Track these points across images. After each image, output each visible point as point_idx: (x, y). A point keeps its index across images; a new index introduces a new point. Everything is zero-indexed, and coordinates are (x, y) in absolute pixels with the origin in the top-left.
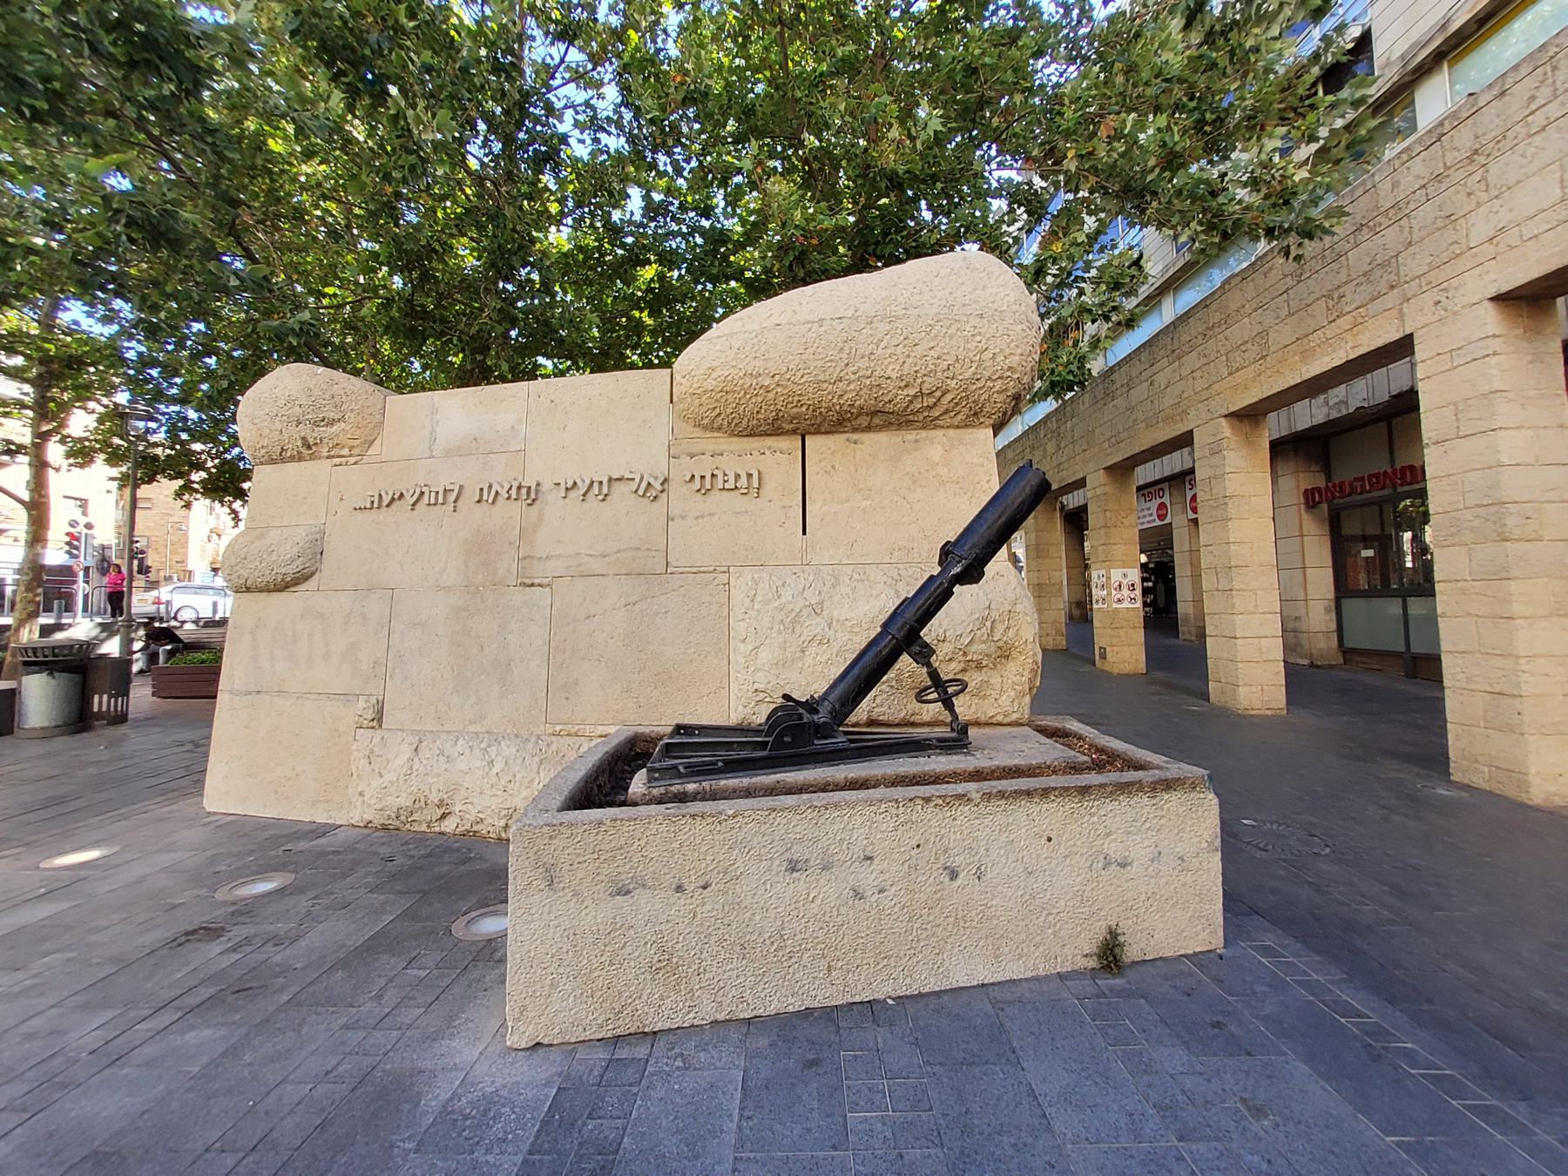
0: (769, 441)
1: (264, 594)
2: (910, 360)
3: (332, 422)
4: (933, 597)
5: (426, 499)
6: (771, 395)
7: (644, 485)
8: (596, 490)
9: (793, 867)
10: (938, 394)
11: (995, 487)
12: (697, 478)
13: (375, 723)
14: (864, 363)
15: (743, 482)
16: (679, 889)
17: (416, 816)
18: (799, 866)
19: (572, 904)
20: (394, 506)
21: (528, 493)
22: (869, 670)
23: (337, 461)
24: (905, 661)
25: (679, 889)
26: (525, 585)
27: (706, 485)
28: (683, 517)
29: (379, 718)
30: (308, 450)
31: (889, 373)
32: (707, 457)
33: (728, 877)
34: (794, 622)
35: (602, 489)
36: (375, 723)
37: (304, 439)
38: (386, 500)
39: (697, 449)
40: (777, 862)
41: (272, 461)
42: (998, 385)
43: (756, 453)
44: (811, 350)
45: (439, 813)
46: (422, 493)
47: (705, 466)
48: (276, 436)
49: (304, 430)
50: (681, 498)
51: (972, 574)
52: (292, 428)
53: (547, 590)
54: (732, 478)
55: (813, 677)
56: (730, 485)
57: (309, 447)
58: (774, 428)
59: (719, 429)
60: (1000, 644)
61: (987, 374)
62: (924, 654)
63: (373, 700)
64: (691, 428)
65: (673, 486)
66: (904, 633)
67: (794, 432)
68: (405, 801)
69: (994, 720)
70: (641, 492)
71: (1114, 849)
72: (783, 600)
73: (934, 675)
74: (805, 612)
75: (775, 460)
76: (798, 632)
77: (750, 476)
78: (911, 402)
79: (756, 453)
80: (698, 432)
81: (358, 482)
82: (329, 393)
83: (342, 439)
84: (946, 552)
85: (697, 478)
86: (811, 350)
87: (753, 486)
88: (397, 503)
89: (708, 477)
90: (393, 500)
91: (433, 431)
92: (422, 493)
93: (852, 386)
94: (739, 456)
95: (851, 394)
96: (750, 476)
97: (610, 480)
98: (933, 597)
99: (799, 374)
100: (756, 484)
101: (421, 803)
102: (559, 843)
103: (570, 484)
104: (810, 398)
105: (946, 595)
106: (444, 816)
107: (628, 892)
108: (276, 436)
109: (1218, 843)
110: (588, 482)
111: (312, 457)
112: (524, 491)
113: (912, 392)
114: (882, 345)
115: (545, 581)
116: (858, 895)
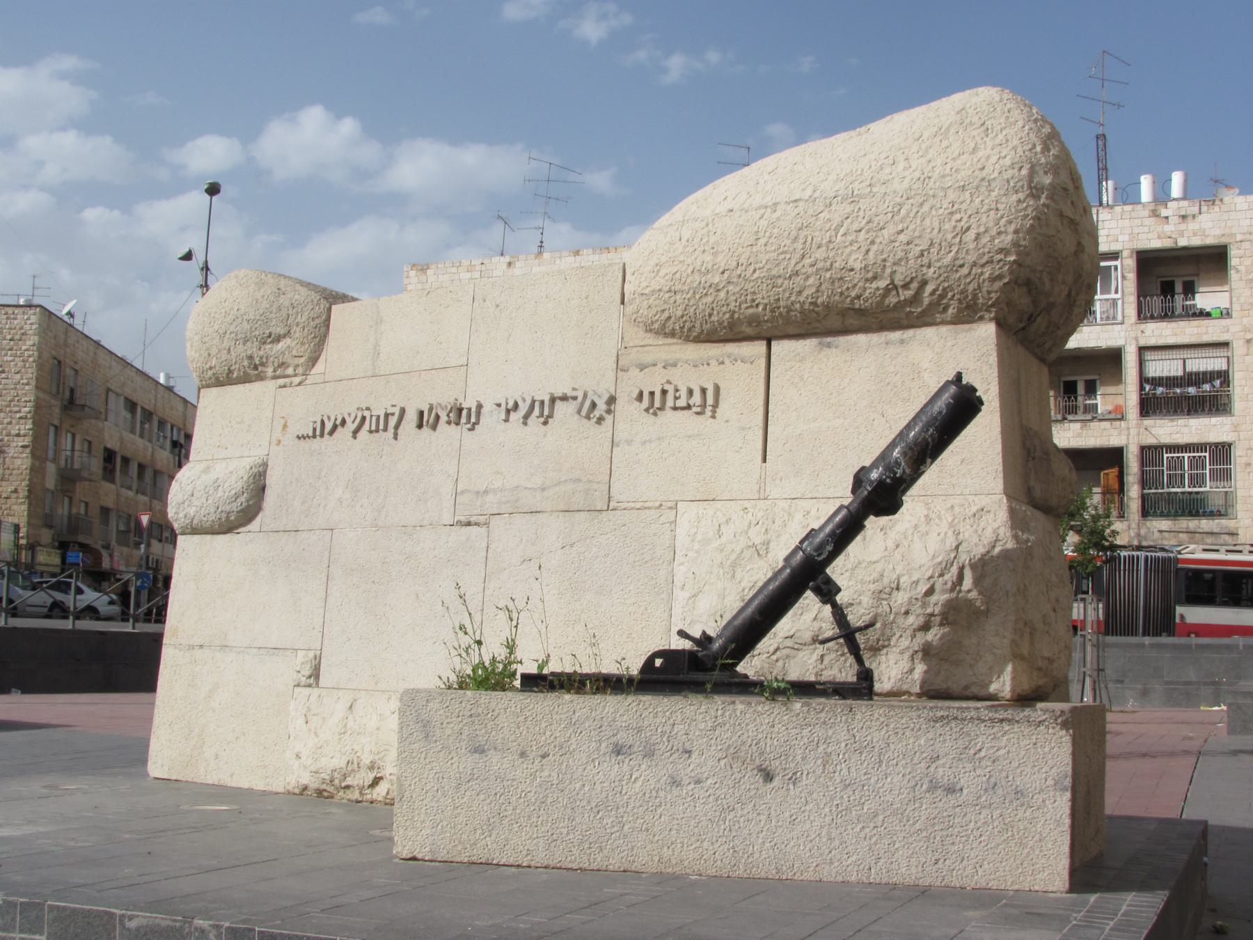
0: (731, 348)
1: (209, 537)
2: (874, 248)
3: (278, 339)
4: (847, 530)
5: (366, 426)
6: (722, 294)
7: (587, 404)
8: (537, 411)
9: (618, 750)
10: (914, 285)
13: (312, 681)
14: (820, 254)
15: (697, 399)
17: (349, 781)
18: (624, 750)
19: (442, 754)
20: (335, 435)
23: (281, 381)
26: (460, 523)
27: (655, 402)
28: (629, 442)
29: (316, 674)
30: (251, 373)
31: (851, 262)
33: (563, 751)
34: (734, 566)
36: (312, 681)
37: (251, 358)
40: (604, 745)
41: (218, 383)
42: (987, 272)
43: (713, 363)
44: (762, 241)
46: (364, 418)
47: (653, 381)
48: (224, 356)
49: (252, 348)
50: (628, 409)
52: (241, 348)
53: (483, 530)
55: (708, 611)
56: (682, 403)
57: (256, 368)
59: (672, 334)
61: (971, 258)
62: (828, 592)
63: (311, 654)
64: (641, 334)
65: (619, 406)
66: (808, 574)
68: (339, 762)
69: (968, 693)
70: (584, 412)
71: (942, 773)
72: (724, 539)
73: (839, 615)
74: (747, 554)
76: (738, 576)
77: (704, 391)
79: (713, 363)
80: (650, 339)
81: (302, 403)
82: (275, 306)
83: (287, 358)
86: (762, 241)
87: (707, 402)
88: (339, 429)
91: (376, 346)
92: (364, 418)
93: (811, 281)
94: (693, 365)
95: (808, 290)
96: (704, 391)
99: (751, 268)
100: (710, 400)
101: (352, 766)
103: (511, 405)
104: (764, 296)
106: (376, 782)
107: (483, 751)
108: (224, 356)
109: (1068, 782)
110: (529, 402)
111: (260, 378)
112: (464, 413)
113: (882, 284)
114: (842, 231)
115: (482, 519)
116: (675, 783)
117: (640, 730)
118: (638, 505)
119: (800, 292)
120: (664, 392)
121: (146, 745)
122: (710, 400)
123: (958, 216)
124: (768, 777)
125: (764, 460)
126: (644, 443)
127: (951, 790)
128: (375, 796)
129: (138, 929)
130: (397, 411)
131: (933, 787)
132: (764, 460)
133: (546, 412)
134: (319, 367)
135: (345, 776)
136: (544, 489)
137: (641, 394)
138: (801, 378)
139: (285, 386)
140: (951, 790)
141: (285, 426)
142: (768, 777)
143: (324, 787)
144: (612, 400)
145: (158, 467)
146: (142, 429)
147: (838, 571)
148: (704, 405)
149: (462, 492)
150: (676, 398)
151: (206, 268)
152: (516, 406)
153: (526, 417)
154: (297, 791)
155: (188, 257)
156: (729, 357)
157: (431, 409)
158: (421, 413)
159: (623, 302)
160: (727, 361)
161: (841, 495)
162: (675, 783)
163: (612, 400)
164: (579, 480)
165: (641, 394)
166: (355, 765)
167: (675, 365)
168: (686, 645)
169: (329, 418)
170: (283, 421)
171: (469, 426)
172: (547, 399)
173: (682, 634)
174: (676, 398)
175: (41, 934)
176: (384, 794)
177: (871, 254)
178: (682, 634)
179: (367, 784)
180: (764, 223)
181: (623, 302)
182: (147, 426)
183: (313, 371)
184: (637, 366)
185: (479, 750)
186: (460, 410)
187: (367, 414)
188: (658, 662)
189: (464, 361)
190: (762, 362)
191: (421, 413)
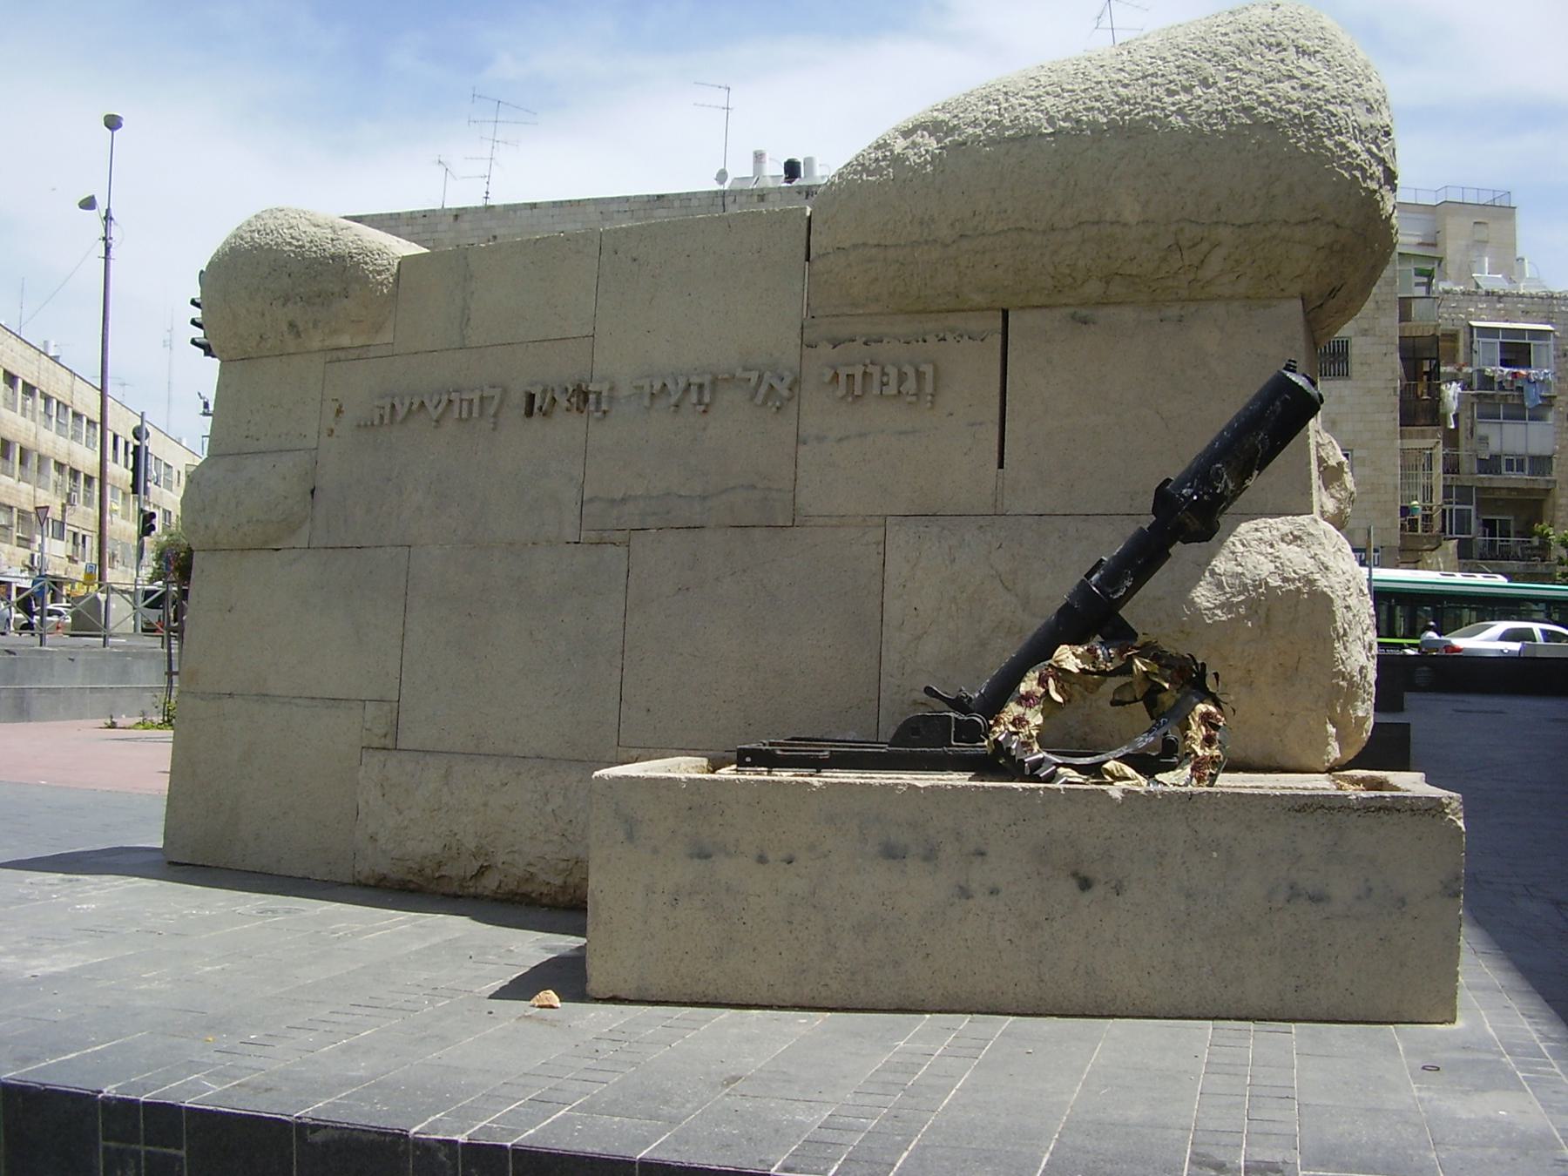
10: (1205, 246)
12: (842, 378)
15: (910, 385)
16: (762, 860)
21: (598, 403)
25: (762, 860)
35: (701, 392)
38: (402, 411)
43: (931, 339)
45: (476, 865)
46: (393, 406)
53: (622, 550)
70: (759, 399)
77: (920, 375)
78: (1164, 259)
79: (931, 339)
84: (1164, 498)
85: (842, 378)
89: (858, 378)
97: (714, 382)
100: (929, 388)
103: (657, 386)
107: (708, 856)
115: (618, 536)
116: (965, 893)
118: (834, 521)
119: (1055, 252)
122: (929, 388)
124: (1085, 884)
125: (1001, 466)
126: (840, 440)
127: (1317, 899)
128: (480, 890)
129: (326, 1145)
130: (497, 392)
131: (1294, 893)
132: (1001, 466)
133: (707, 399)
135: (440, 864)
136: (704, 498)
137: (836, 375)
140: (1317, 899)
141: (339, 411)
142: (1085, 884)
143: (410, 877)
144: (796, 382)
145: (43, 451)
146: (24, 408)
149: (591, 500)
150: (883, 384)
151: (108, 218)
154: (372, 882)
155: (88, 204)
156: (952, 331)
157: (544, 391)
158: (531, 397)
159: (808, 259)
160: (949, 337)
162: (965, 893)
163: (796, 382)
164: (754, 487)
165: (836, 375)
166: (454, 851)
170: (337, 405)
171: (599, 414)
172: (707, 379)
174: (883, 384)
175: (179, 1148)
176: (494, 886)
179: (469, 875)
181: (808, 259)
182: (29, 402)
184: (829, 341)
185: (704, 855)
186: (586, 394)
187: (454, 396)
189: (588, 330)
190: (997, 340)
191: (531, 397)
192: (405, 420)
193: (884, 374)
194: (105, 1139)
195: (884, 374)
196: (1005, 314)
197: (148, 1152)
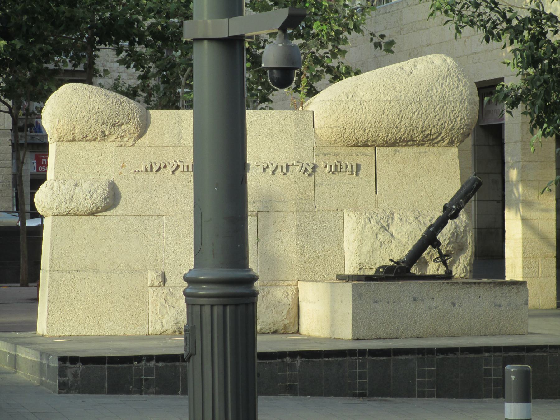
0: (360, 149)
4: (441, 224)
5: (180, 169)
8: (279, 170)
11: (459, 187)
15: (349, 168)
22: (416, 255)
24: (429, 248)
25: (388, 302)
32: (332, 156)
38: (155, 168)
39: (327, 152)
43: (354, 155)
46: (178, 166)
50: (322, 173)
51: (455, 216)
54: (344, 166)
55: (398, 251)
58: (365, 145)
60: (460, 244)
67: (372, 146)
71: (497, 301)
75: (364, 157)
77: (352, 166)
79: (354, 155)
88: (162, 170)
90: (160, 168)
91: (180, 132)
92: (178, 166)
96: (352, 166)
98: (441, 224)
100: (355, 170)
102: (362, 288)
103: (265, 166)
105: (445, 223)
110: (275, 166)
116: (430, 308)
117: (420, 293)
120: (336, 166)
121: (36, 322)
123: (455, 112)
125: (376, 194)
131: (495, 306)
132: (376, 194)
134: (144, 139)
137: (326, 165)
138: (389, 163)
139: (121, 146)
140: (500, 306)
141: (123, 166)
147: (440, 237)
148: (352, 172)
150: (341, 168)
152: (268, 167)
153: (273, 172)
160: (360, 155)
161: (438, 213)
165: (326, 165)
167: (338, 155)
168: (392, 263)
169: (156, 164)
173: (391, 260)
174: (341, 168)
177: (426, 123)
178: (391, 260)
180: (387, 107)
181: (314, 127)
183: (139, 141)
188: (381, 270)
192: (158, 171)
193: (341, 165)
194: (418, 378)
195: (341, 165)
196: (375, 148)
197: (349, 369)
